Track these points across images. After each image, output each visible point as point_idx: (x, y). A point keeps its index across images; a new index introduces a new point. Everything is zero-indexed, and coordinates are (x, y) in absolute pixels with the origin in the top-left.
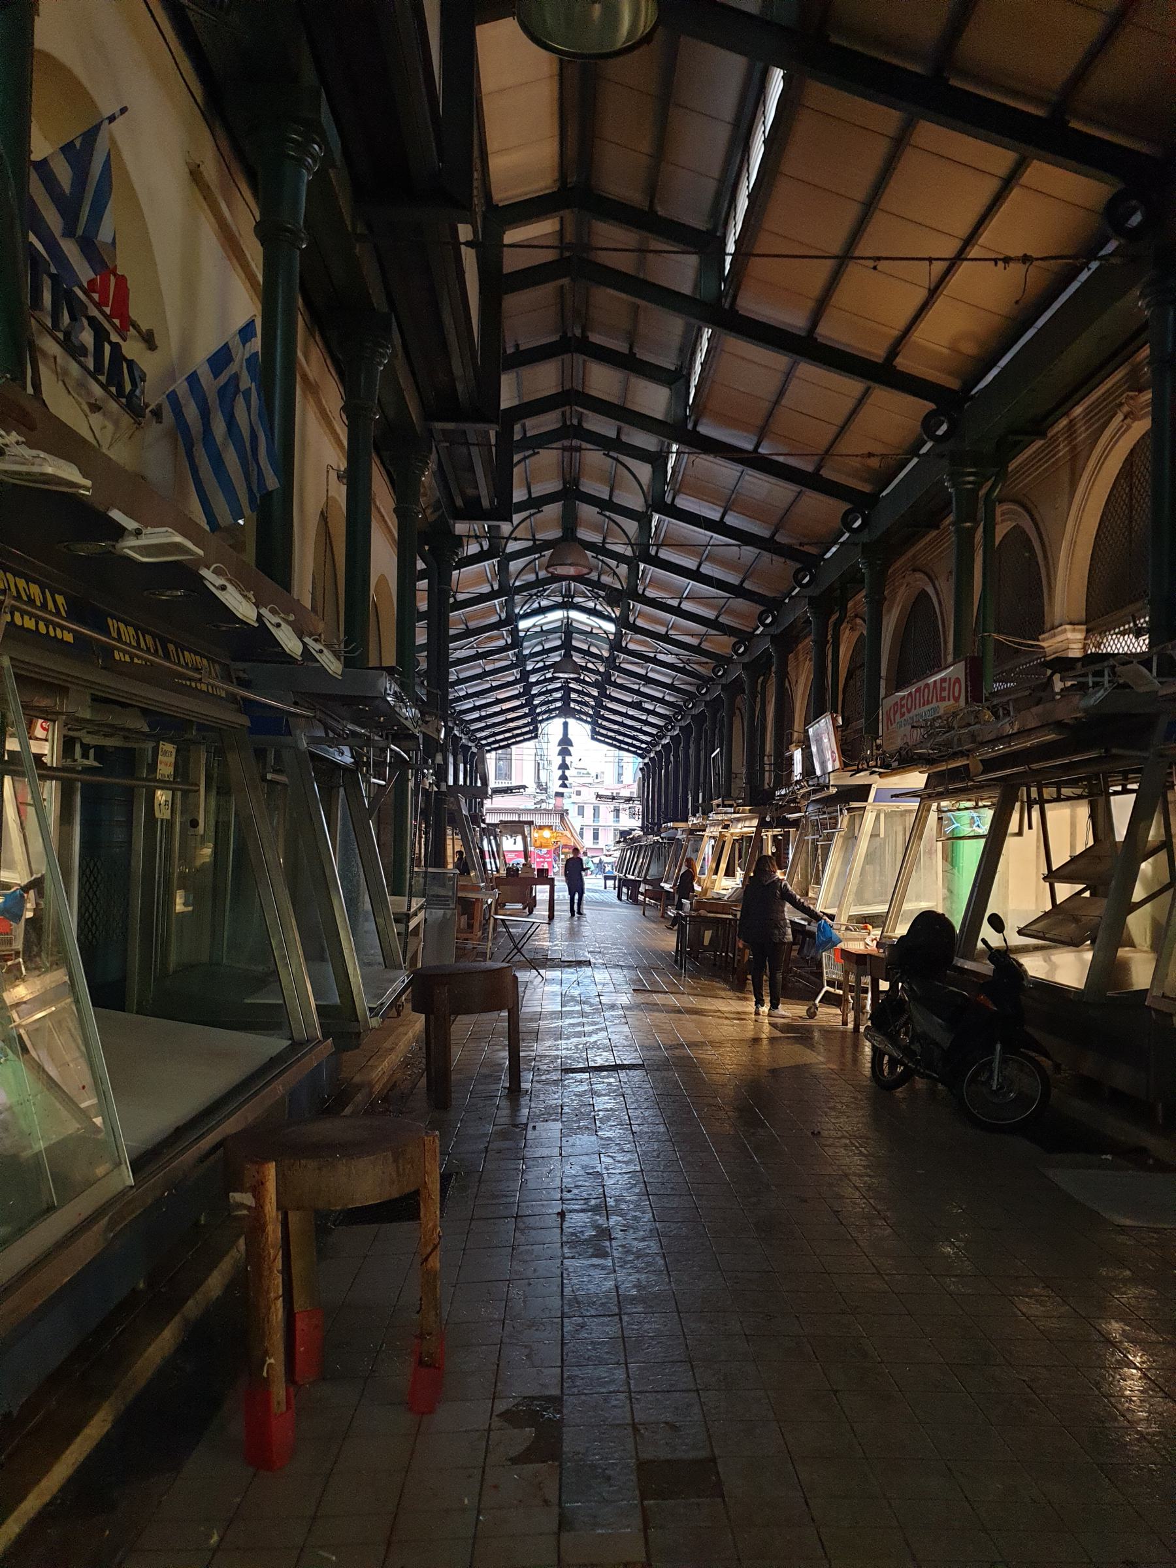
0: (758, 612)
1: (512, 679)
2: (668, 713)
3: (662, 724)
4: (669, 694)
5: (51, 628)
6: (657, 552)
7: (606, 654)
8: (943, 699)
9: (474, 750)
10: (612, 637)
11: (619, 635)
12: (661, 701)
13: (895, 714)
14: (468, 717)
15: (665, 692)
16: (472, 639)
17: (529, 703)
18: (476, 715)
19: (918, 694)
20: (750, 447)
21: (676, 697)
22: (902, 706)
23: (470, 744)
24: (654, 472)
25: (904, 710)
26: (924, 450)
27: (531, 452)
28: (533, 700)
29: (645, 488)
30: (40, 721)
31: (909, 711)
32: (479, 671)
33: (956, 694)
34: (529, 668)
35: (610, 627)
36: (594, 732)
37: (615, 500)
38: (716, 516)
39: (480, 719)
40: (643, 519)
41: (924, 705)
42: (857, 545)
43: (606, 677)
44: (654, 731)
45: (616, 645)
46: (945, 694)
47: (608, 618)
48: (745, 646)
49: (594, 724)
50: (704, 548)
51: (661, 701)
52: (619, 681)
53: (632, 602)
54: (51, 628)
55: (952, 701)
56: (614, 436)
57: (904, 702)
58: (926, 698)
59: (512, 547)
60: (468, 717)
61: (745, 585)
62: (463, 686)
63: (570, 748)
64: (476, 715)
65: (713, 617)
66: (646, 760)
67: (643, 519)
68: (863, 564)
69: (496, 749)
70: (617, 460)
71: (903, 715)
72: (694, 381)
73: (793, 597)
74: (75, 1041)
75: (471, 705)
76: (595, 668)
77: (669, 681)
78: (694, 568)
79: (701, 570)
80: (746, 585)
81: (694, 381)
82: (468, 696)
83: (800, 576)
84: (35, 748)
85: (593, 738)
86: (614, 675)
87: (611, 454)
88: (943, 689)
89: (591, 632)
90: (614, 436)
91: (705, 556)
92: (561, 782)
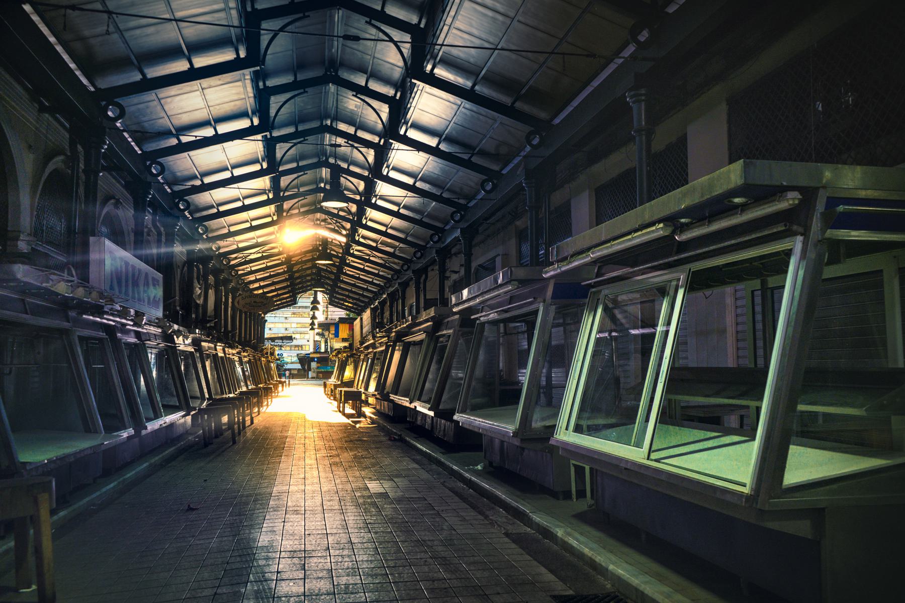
0: (451, 212)
2: (375, 290)
12: (377, 275)
14: (252, 287)
18: (256, 285)
44: (367, 300)
51: (372, 283)
56: (353, 133)
60: (252, 287)
61: (443, 195)
63: (318, 306)
64: (256, 285)
67: (249, 567)
68: (525, 184)
74: (298, 384)
75: (254, 278)
77: (376, 272)
82: (252, 272)
87: (373, 22)
90: (353, 133)
92: (311, 327)
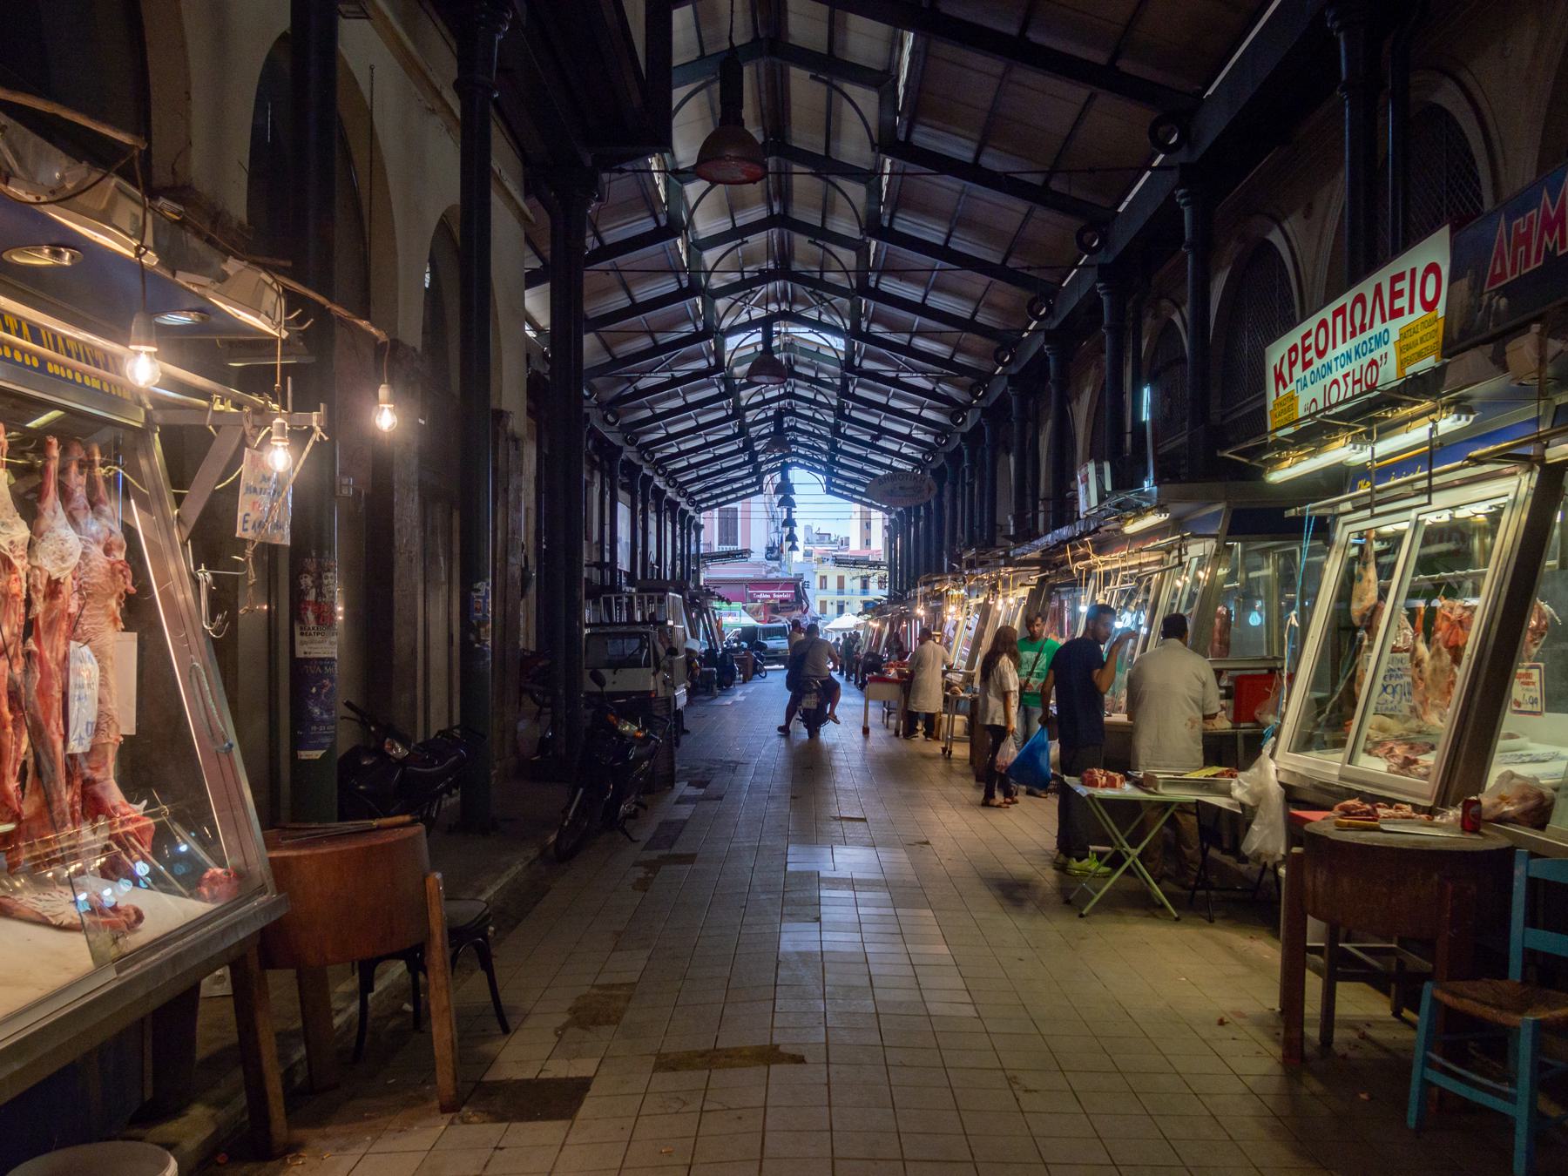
1: (730, 432)
3: (929, 439)
4: (917, 428)
5: (27, 357)
6: (877, 282)
7: (834, 403)
8: (1397, 313)
9: (691, 513)
10: (842, 357)
11: (850, 353)
12: (908, 438)
13: (1292, 364)
15: (911, 426)
16: (663, 357)
17: (743, 431)
19: (1339, 319)
20: (1013, 30)
21: (914, 449)
22: (1306, 350)
23: (679, 499)
24: (858, 258)
25: (1311, 354)
26: (1031, 328)
27: (739, 241)
28: (761, 468)
29: (861, 216)
30: (1106, 719)
31: (1321, 354)
32: (692, 424)
33: (1430, 296)
34: (749, 420)
35: (839, 343)
36: (829, 483)
37: (829, 227)
38: (967, 155)
39: (699, 479)
40: (860, 248)
41: (1353, 335)
42: (1093, 266)
43: (835, 429)
45: (848, 365)
46: (1398, 304)
47: (834, 330)
48: (947, 439)
49: (830, 473)
50: (929, 273)
51: (908, 438)
52: (849, 432)
53: (874, 243)
54: (27, 357)
55: (1419, 312)
57: (1311, 340)
58: (1358, 323)
59: (716, 282)
62: (673, 442)
65: (967, 316)
66: (893, 516)
69: (718, 505)
70: (823, 247)
71: (1306, 365)
72: (872, 252)
73: (1076, 267)
76: (826, 401)
78: (941, 243)
79: (927, 302)
80: (980, 318)
81: (872, 252)
82: (681, 454)
83: (1035, 308)
84: (310, 583)
85: (829, 492)
86: (844, 425)
88: (1396, 295)
89: (818, 352)
91: (930, 285)
